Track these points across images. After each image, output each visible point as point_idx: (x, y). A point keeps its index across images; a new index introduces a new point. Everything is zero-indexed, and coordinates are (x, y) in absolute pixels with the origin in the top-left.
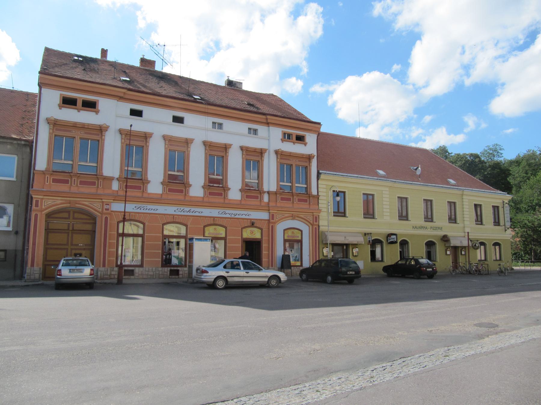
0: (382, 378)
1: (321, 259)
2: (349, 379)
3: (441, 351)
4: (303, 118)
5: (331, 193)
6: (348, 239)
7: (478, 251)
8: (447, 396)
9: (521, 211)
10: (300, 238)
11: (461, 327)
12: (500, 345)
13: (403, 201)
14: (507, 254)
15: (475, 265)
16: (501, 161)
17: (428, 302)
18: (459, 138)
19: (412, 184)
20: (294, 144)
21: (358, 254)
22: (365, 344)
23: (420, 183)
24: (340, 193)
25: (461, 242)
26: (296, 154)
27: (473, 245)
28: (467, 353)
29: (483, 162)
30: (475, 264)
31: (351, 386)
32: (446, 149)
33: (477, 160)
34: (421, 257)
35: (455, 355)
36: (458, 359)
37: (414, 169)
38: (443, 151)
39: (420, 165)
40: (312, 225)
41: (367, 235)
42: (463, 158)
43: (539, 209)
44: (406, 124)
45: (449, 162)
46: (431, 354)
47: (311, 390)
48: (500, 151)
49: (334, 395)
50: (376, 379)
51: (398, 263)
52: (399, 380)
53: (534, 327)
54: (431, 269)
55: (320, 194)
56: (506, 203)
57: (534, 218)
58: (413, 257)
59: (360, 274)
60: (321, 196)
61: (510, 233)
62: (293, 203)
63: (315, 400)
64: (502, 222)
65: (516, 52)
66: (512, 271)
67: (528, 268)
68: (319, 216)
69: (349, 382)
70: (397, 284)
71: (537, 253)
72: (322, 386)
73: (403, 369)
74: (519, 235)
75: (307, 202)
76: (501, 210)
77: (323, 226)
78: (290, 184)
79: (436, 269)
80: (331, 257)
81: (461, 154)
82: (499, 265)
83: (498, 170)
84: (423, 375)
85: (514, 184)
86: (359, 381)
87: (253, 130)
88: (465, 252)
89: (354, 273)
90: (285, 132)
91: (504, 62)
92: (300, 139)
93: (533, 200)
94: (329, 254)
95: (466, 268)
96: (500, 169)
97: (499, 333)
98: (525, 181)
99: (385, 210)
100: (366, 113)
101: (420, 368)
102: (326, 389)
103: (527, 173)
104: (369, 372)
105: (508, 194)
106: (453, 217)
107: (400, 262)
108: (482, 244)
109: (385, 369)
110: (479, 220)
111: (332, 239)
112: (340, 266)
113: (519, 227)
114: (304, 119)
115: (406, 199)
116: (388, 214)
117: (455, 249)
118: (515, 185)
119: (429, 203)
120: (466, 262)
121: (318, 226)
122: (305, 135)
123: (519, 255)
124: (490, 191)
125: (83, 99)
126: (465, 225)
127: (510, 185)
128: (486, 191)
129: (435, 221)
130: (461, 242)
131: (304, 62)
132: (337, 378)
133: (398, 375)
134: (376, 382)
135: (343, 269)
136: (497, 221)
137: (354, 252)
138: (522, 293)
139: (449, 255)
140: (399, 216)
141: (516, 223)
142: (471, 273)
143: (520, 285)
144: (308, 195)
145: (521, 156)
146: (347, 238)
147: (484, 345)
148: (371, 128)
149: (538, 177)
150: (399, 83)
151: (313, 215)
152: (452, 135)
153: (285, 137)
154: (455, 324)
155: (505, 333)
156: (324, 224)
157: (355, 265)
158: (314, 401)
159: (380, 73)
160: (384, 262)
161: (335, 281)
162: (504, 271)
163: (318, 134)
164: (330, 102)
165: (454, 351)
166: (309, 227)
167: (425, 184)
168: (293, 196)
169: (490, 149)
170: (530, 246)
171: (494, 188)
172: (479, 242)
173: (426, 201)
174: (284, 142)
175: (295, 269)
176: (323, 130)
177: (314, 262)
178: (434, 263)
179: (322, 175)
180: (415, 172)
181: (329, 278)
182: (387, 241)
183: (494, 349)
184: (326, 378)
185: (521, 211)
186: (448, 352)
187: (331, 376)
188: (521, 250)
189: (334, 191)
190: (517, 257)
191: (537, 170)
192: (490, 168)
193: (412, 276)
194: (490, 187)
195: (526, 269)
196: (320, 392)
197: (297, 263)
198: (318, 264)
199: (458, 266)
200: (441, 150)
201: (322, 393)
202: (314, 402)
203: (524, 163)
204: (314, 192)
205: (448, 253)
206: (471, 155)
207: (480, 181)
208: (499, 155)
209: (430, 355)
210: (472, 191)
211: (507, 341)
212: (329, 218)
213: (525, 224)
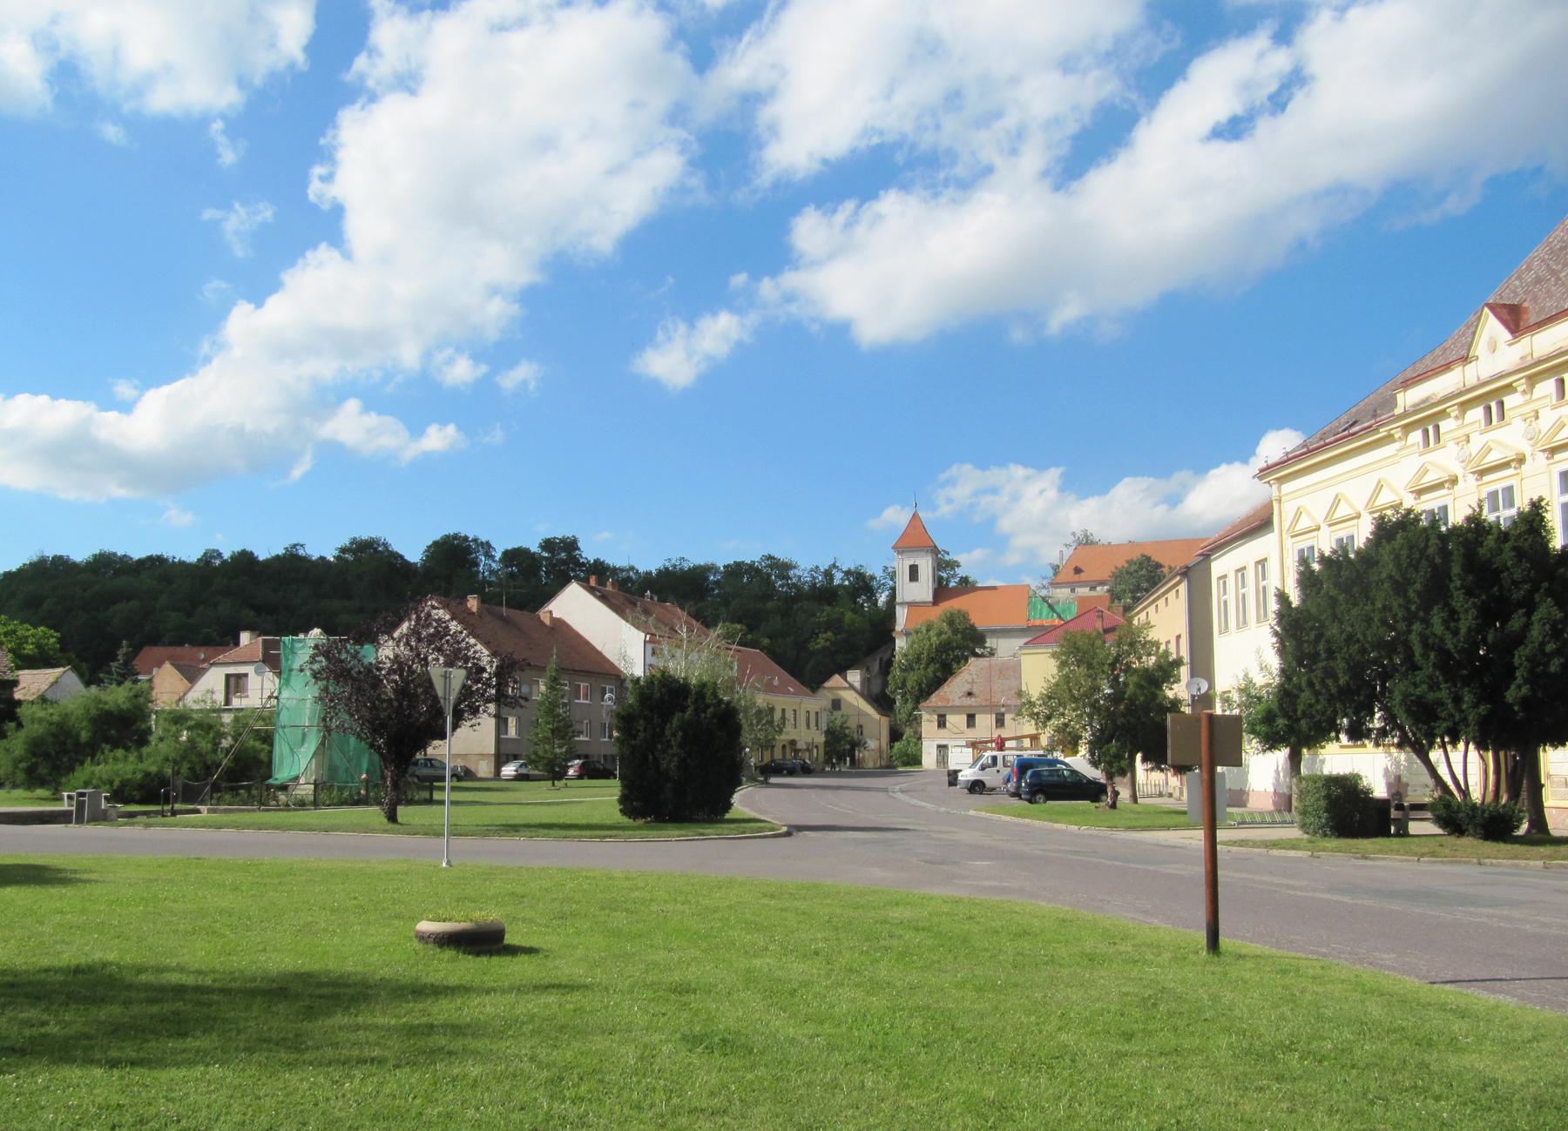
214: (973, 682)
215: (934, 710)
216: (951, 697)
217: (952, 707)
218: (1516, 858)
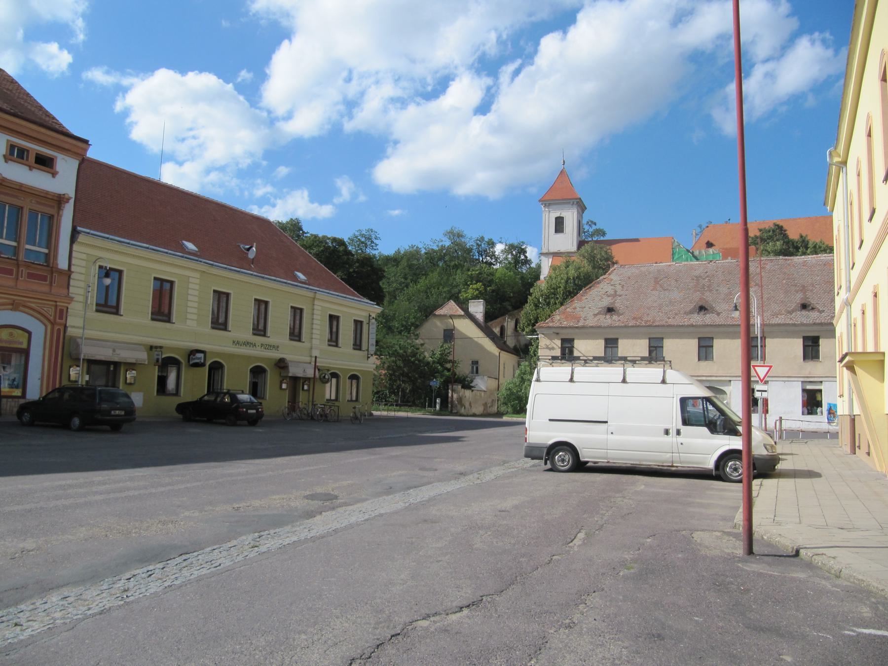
0: (143, 590)
1: (63, 386)
2: (84, 597)
3: (248, 539)
4: (54, 124)
5: (95, 269)
6: (119, 355)
7: (328, 385)
8: (244, 609)
9: (393, 332)
10: (25, 346)
11: (285, 500)
12: (335, 525)
13: (222, 298)
14: (367, 390)
15: (321, 406)
16: (374, 256)
17: (241, 463)
18: (325, 211)
19: (239, 271)
20: (30, 169)
21: (135, 380)
22: (123, 534)
23: (252, 273)
24: (112, 273)
25: (304, 370)
26: (31, 189)
27: (322, 377)
28: (287, 540)
29: (350, 253)
30: (321, 405)
31: (83, 610)
32: (300, 224)
33: (341, 249)
34: (241, 392)
35: (270, 543)
36: (271, 550)
37: (245, 249)
38: (295, 227)
39: (255, 244)
40: (53, 324)
41: (154, 350)
42: (321, 242)
43: (414, 331)
44: (248, 174)
45: (301, 246)
46: (233, 545)
47: (5, 624)
48: (375, 241)
49: (49, 628)
50: (132, 592)
51: (203, 399)
52: (171, 591)
53: (384, 497)
54: (254, 411)
55: (73, 269)
56: (373, 318)
57: (408, 343)
58: (229, 390)
59: (135, 415)
60: (76, 272)
61: (374, 361)
62: (17, 279)
63: (9, 641)
64: (364, 346)
65: (418, 99)
66: (371, 417)
67: (392, 414)
68: (67, 308)
69: (82, 602)
70: (198, 432)
71: (406, 392)
72: (28, 614)
73: (183, 572)
74: (386, 366)
75: (12, 275)
76: (365, 327)
77: (74, 327)
78: (14, 244)
79: (262, 411)
80: (84, 383)
81: (320, 235)
82: (353, 408)
83: (369, 268)
84: (213, 579)
85: (388, 292)
86: (101, 599)
87: (18, 149)
88: (309, 387)
89: (123, 413)
90: (14, 144)
91: (401, 109)
92: (44, 163)
93: (409, 318)
94: (80, 379)
95: (307, 411)
96: (372, 266)
97: (337, 507)
98: (403, 289)
99: (189, 310)
100: (183, 140)
101: (210, 568)
102: (34, 619)
103: (406, 279)
104: (122, 581)
105: (377, 304)
106: (297, 330)
107: (206, 398)
108: (335, 375)
109: (151, 575)
110: (334, 340)
111: (88, 351)
112: (97, 401)
113: (387, 354)
114: (57, 127)
115: (228, 295)
116: (195, 317)
117: (295, 381)
118: (389, 293)
119: (262, 306)
120: (309, 401)
121: (63, 327)
122: (56, 157)
123: (383, 394)
124: (353, 298)
125: (12, 143)
126: (313, 345)
127: (382, 292)
128: (347, 296)
129: (268, 336)
130: (304, 370)
131: (81, 19)
132: (60, 598)
133: (172, 584)
134: (131, 598)
135: (103, 406)
136: (358, 343)
137: (71, 373)
138: (377, 449)
139: (284, 389)
140: (212, 323)
141: (383, 348)
142: (314, 419)
143: (378, 437)
144: (49, 268)
145: (402, 252)
146: (118, 351)
147: (313, 527)
148: (188, 168)
149: (419, 286)
150: (247, 104)
151: (56, 306)
152: (316, 205)
153: (12, 153)
154: (277, 497)
155: (345, 507)
156: (75, 324)
157: (126, 400)
158: (6, 644)
159: (217, 79)
160: (180, 396)
161: (86, 427)
162: (359, 416)
163: (80, 159)
164: (119, 106)
165: (267, 539)
166: (46, 326)
167: (260, 275)
168: (18, 266)
169: (362, 235)
170: (398, 382)
171: (360, 294)
172: (330, 372)
173: (258, 302)
174: (10, 162)
175: (9, 404)
176: (91, 154)
177: (50, 390)
178: (260, 401)
179: (80, 235)
180: (245, 253)
181: (76, 421)
182: (189, 361)
183: (326, 531)
184: (39, 600)
185: (393, 332)
186: (258, 540)
187: (49, 594)
188: (385, 386)
189: (101, 267)
190: (380, 398)
191: (419, 275)
192: (358, 263)
193: (224, 421)
194: (354, 291)
195: (389, 415)
196: (22, 625)
197: (14, 392)
198: (57, 395)
199: (297, 406)
200: (291, 225)
201: (24, 628)
202: (6, 646)
203: (404, 263)
204: (63, 264)
205: (284, 386)
206: (334, 240)
207: (341, 281)
208: (373, 246)
209: (229, 546)
210: (329, 295)
211: (346, 518)
212: (87, 313)
213: (396, 350)
214: (615, 295)
215: (555, 332)
216: (583, 315)
217: (583, 327)
218: (512, 417)
